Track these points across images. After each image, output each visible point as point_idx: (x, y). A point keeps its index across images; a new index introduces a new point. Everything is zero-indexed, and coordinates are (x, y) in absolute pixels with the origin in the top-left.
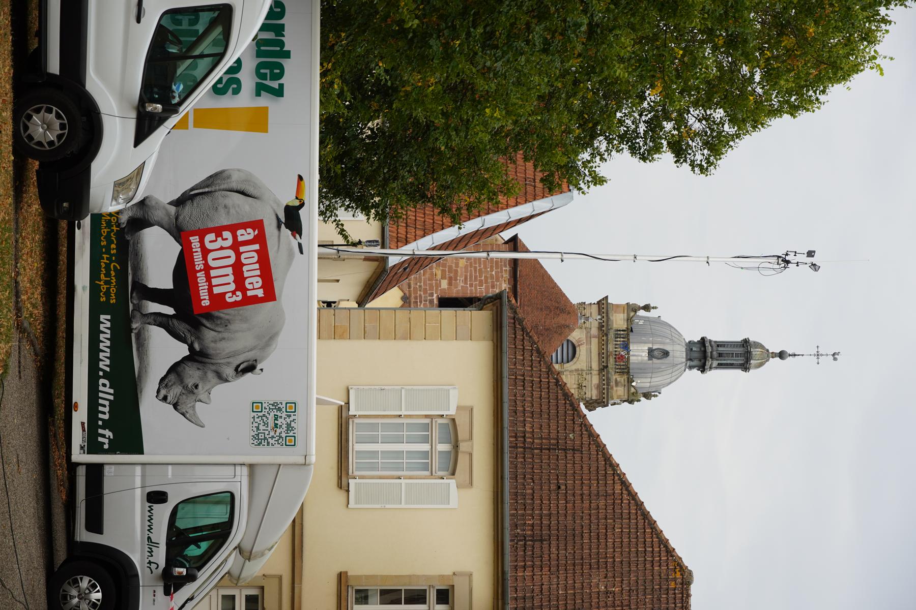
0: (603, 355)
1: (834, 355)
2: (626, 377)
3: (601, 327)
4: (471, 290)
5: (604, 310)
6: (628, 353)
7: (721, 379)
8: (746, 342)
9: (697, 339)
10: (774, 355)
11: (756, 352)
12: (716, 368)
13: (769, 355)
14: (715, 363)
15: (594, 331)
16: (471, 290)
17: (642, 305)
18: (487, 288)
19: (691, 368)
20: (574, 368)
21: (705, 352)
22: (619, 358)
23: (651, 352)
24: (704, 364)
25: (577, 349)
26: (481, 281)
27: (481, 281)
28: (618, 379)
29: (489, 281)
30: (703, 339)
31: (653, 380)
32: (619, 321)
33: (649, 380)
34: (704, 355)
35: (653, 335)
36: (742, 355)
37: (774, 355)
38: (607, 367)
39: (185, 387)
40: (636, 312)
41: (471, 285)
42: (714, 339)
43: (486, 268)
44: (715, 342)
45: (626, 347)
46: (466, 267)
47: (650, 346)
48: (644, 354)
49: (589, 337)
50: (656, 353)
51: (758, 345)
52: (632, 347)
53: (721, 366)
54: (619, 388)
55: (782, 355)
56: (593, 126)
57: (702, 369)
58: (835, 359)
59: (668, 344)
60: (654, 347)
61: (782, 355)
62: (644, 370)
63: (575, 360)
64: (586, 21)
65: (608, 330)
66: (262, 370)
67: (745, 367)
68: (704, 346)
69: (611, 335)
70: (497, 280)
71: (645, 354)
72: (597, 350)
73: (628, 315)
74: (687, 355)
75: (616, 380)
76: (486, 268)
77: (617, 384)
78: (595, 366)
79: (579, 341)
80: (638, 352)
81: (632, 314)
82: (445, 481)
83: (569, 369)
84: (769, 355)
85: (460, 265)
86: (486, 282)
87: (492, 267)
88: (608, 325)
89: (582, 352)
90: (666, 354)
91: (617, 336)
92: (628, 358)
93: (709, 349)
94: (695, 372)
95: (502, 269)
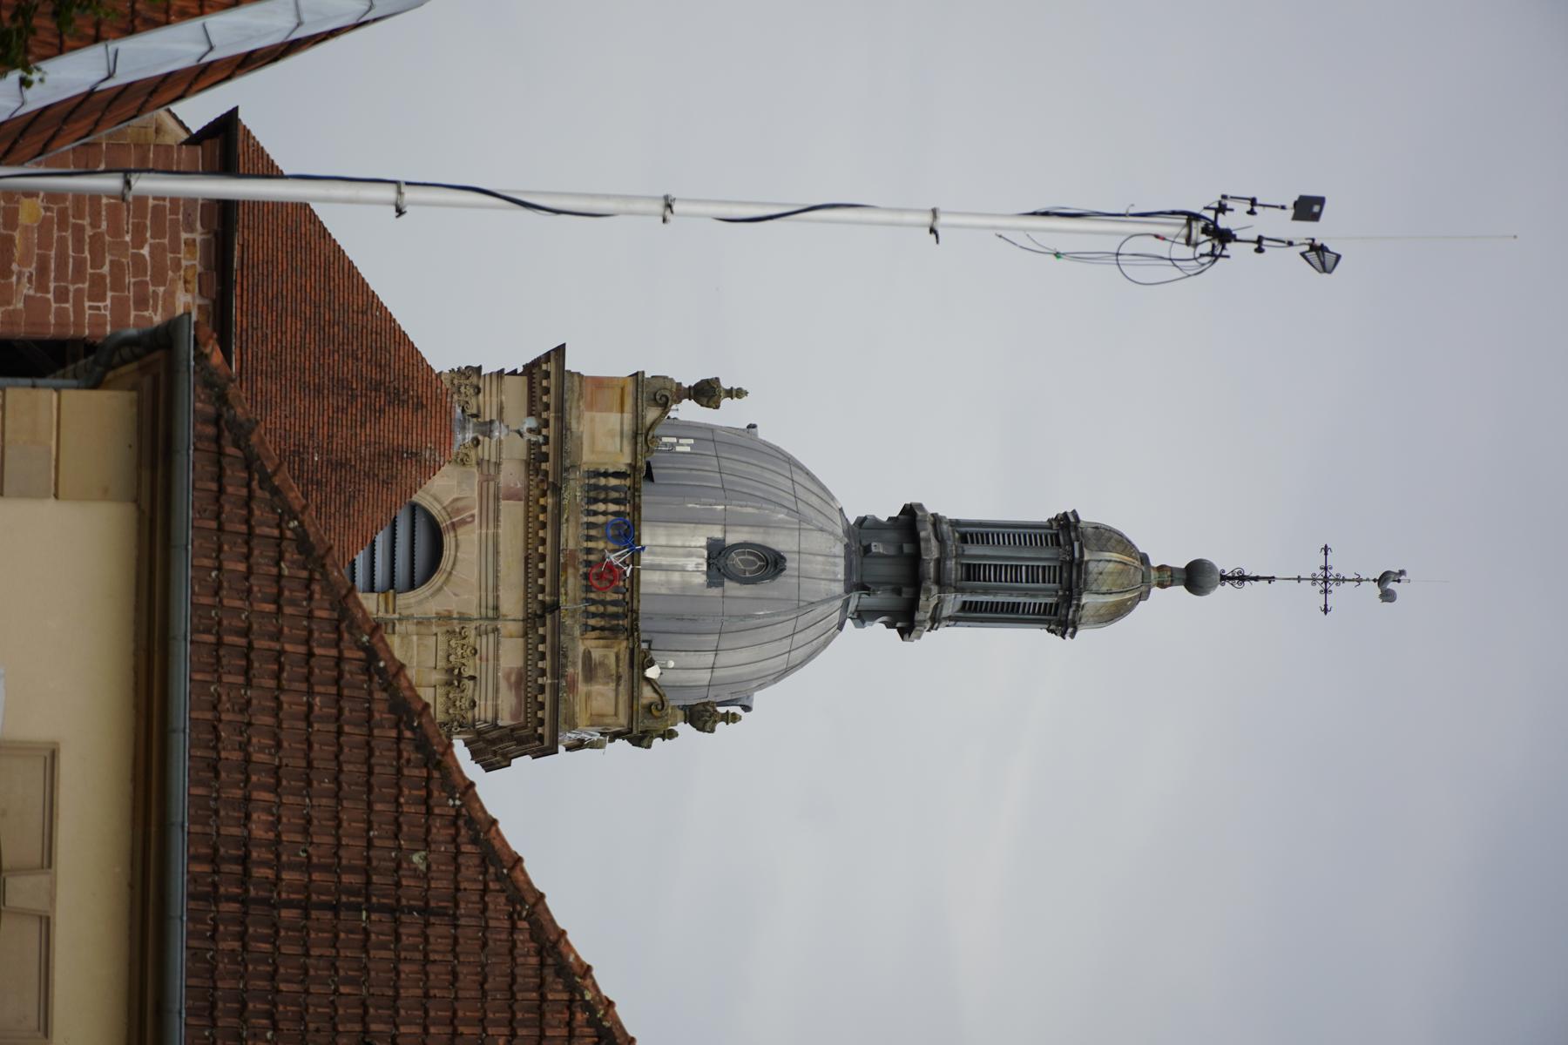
0: (541, 564)
1: (1383, 579)
2: (623, 646)
3: (535, 460)
4: (61, 313)
5: (550, 399)
6: (635, 558)
10: (1168, 577)
11: (1101, 563)
12: (954, 620)
13: (1147, 575)
14: (952, 602)
15: (512, 474)
16: (61, 313)
17: (689, 381)
18: (119, 306)
19: (862, 617)
20: (433, 607)
21: (915, 559)
22: (600, 575)
23: (717, 554)
25: (448, 540)
26: (97, 281)
27: (97, 281)
28: (596, 655)
29: (130, 279)
30: (910, 513)
31: (724, 658)
32: (602, 439)
33: (709, 658)
34: (912, 571)
35: (726, 492)
36: (1051, 574)
37: (1168, 577)
38: (555, 607)
40: (665, 407)
41: (61, 296)
42: (950, 512)
43: (116, 230)
44: (955, 524)
45: (627, 534)
46: (45, 226)
47: (717, 533)
48: (691, 563)
49: (492, 498)
50: (736, 560)
51: (1109, 538)
52: (649, 536)
53: (972, 613)
54: (596, 688)
55: (1195, 577)
57: (906, 622)
58: (1388, 596)
59: (779, 526)
61: (1195, 577)
62: (688, 622)
63: (438, 579)
65: (563, 470)
68: (914, 538)
69: (574, 490)
70: (159, 278)
71: (696, 565)
72: (520, 543)
73: (638, 416)
75: (587, 655)
76: (116, 230)
78: (512, 603)
79: (454, 509)
80: (673, 556)
81: (652, 414)
83: (417, 612)
84: (1147, 575)
85: (24, 218)
86: (118, 284)
87: (139, 231)
88: (561, 451)
90: (772, 563)
91: (594, 494)
93: (931, 551)
94: (879, 633)
95: (175, 239)
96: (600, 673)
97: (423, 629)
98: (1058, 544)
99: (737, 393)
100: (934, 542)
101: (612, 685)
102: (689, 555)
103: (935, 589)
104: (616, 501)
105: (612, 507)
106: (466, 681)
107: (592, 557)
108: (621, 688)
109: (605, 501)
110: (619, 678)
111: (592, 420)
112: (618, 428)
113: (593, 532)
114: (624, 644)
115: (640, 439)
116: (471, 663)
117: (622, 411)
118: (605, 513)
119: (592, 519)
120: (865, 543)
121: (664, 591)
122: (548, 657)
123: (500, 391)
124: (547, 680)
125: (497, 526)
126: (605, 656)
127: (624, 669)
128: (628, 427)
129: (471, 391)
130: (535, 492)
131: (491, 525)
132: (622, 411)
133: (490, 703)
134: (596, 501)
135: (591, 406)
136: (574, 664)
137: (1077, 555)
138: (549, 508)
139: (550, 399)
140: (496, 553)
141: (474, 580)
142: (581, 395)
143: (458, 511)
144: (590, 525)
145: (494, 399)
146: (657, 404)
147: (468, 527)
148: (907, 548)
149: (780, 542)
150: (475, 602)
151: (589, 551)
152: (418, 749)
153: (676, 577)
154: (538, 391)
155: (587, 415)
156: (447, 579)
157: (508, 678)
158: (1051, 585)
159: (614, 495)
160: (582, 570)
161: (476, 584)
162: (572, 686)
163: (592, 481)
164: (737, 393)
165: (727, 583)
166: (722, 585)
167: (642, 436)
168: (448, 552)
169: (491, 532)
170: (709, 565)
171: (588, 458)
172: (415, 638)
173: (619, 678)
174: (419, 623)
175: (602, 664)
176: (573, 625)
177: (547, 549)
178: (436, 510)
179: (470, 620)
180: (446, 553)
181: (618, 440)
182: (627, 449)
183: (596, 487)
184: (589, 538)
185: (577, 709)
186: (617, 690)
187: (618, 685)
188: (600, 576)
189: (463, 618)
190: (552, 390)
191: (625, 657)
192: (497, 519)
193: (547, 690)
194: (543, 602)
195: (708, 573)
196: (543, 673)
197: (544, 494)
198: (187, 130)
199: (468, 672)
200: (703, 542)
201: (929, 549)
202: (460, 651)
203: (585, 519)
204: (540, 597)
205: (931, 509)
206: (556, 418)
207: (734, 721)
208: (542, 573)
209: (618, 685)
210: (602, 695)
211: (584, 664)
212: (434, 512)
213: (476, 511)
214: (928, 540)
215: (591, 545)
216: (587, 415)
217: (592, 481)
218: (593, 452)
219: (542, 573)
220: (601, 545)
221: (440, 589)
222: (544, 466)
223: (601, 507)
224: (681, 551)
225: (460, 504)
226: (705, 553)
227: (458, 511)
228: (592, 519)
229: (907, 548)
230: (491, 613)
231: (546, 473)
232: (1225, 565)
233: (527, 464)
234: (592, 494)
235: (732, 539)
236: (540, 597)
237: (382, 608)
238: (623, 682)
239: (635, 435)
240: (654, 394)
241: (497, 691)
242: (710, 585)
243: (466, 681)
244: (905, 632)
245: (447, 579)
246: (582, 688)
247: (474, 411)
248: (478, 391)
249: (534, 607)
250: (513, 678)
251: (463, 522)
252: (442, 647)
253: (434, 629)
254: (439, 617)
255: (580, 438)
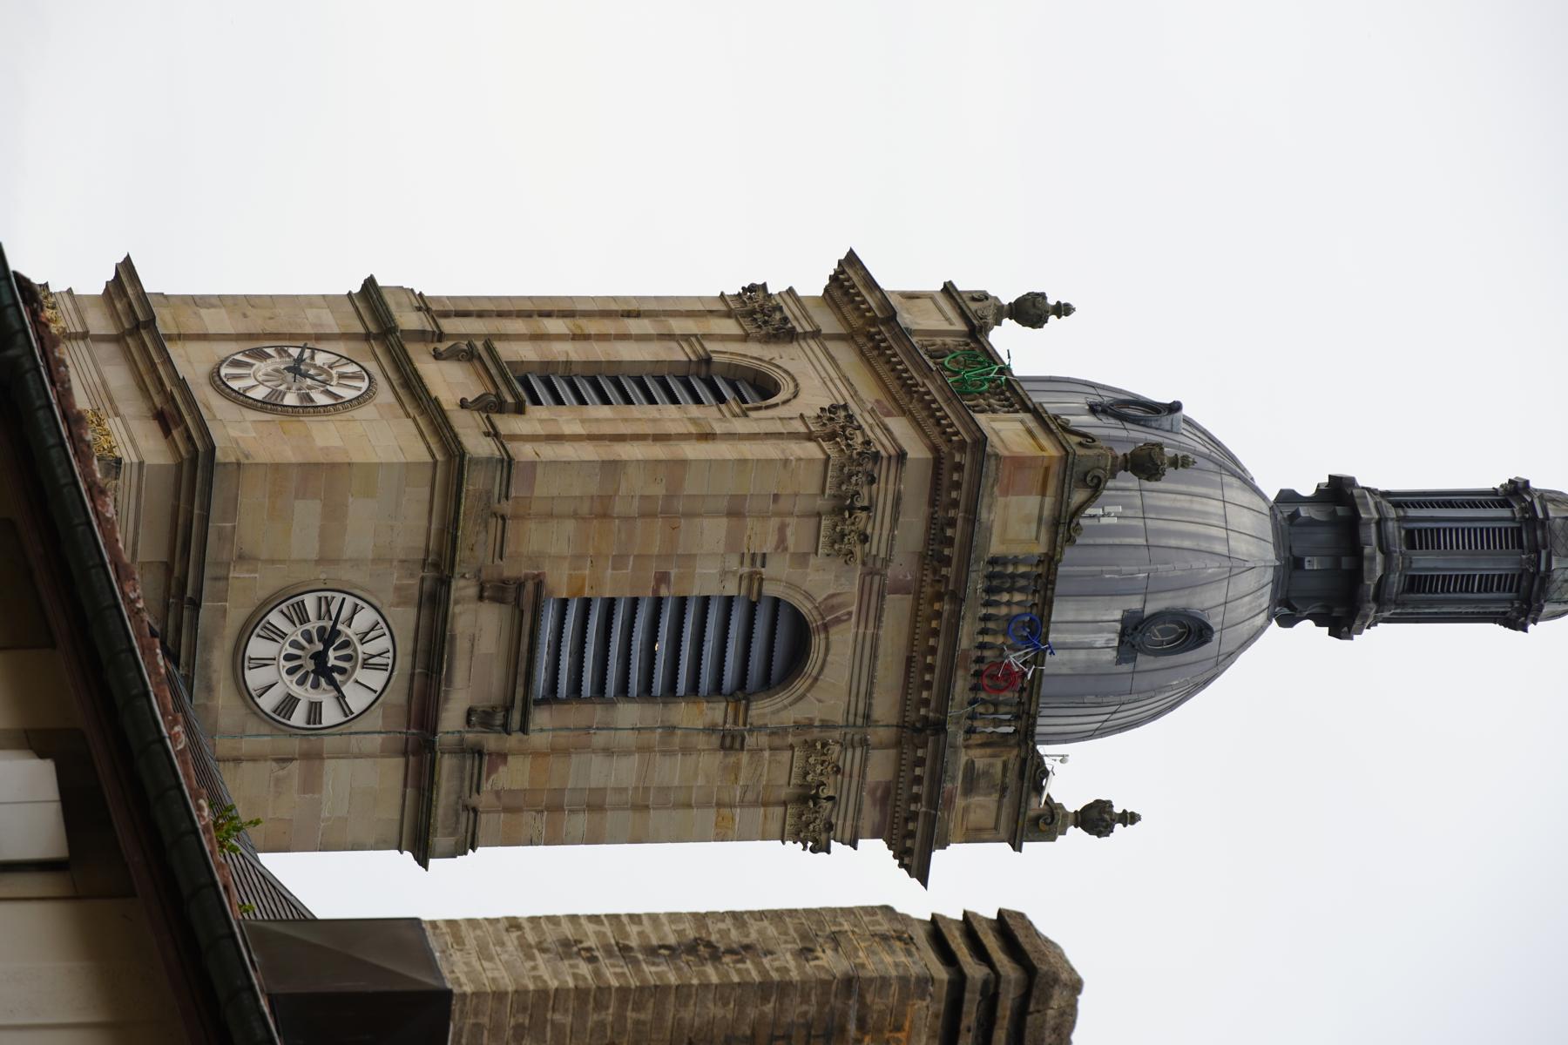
0: (925, 664)
6: (1038, 660)
15: (902, 567)
17: (1007, 298)
18: (821, 1005)
19: (1287, 612)
20: (790, 716)
21: (1355, 575)
22: (991, 677)
25: (817, 642)
28: (980, 764)
38: (939, 727)
45: (1035, 632)
47: (1135, 603)
48: (1100, 640)
54: (976, 799)
56: (1329, 484)
60: (1151, 609)
63: (800, 685)
65: (965, 563)
68: (1356, 550)
69: (976, 582)
71: (1107, 638)
72: (903, 640)
73: (1061, 500)
74: (1276, 582)
75: (970, 765)
77: (972, 781)
78: (885, 707)
79: (829, 606)
80: (1083, 630)
83: (773, 722)
89: (836, 655)
92: (1038, 675)
96: (983, 783)
97: (777, 741)
98: (1521, 546)
100: (1379, 557)
101: (995, 796)
102: (1101, 631)
103: (1373, 606)
104: (1022, 590)
105: (1018, 597)
106: (824, 803)
107: (987, 653)
108: (1005, 800)
109: (1010, 591)
110: (1004, 790)
111: (1006, 506)
112: (1036, 512)
113: (991, 625)
114: (1015, 752)
115: (1061, 529)
116: (831, 781)
117: (1043, 494)
118: (1009, 603)
119: (991, 611)
120: (1296, 552)
121: (1065, 671)
122: (926, 782)
123: (898, 479)
124: (921, 808)
125: (877, 626)
126: (991, 765)
127: (1012, 778)
128: (1046, 513)
129: (862, 478)
130: (928, 590)
131: (871, 625)
132: (1043, 494)
133: (849, 823)
134: (999, 590)
135: (1005, 493)
136: (954, 778)
137: (1543, 568)
138: (945, 615)
139: (918, 827)
140: (874, 656)
141: (843, 683)
142: (996, 480)
143: (833, 609)
144: (986, 618)
145: (891, 487)
146: (1086, 486)
147: (842, 626)
148: (1346, 563)
149: (1203, 601)
150: (842, 706)
151: (982, 646)
152: (765, 999)
153: (1081, 655)
154: (945, 482)
155: (1001, 500)
156: (812, 686)
157: (873, 792)
158: (1507, 595)
159: (1022, 583)
160: (974, 667)
161: (845, 688)
162: (950, 802)
163: (997, 569)
165: (1140, 658)
166: (1134, 659)
167: (1064, 525)
168: (816, 655)
169: (870, 632)
170: (1121, 642)
171: (996, 548)
172: (767, 754)
173: (1004, 790)
174: (773, 734)
175: (986, 773)
176: (956, 733)
177: (938, 660)
178: (805, 608)
179: (834, 727)
180: (813, 656)
181: (1034, 526)
182: (1044, 537)
183: (1000, 575)
184: (984, 632)
185: (952, 826)
186: (1000, 802)
187: (1002, 796)
188: (993, 677)
189: (826, 726)
190: (964, 486)
191: (1014, 766)
192: (878, 618)
193: (921, 818)
194: (926, 718)
195: (1118, 649)
196: (916, 798)
197: (939, 597)
199: (828, 792)
200: (1118, 615)
201: (1372, 570)
202: (819, 768)
203: (984, 611)
204: (923, 711)
206: (966, 520)
207: (1133, 823)
208: (928, 686)
209: (1002, 796)
210: (982, 807)
211: (965, 776)
212: (804, 611)
213: (854, 608)
214: (1373, 558)
215: (988, 639)
216: (1001, 500)
217: (997, 569)
218: (1003, 542)
219: (928, 686)
220: (1000, 640)
221: (802, 697)
222: (944, 571)
223: (1005, 597)
224: (1090, 626)
225: (835, 601)
226: (1119, 626)
227: (833, 609)
228: (991, 611)
229: (1346, 563)
230: (859, 721)
231: (946, 578)
233: (922, 557)
234: (995, 583)
236: (923, 711)
237: (730, 719)
238: (1008, 794)
239: (1056, 523)
241: (858, 811)
242: (1119, 662)
243: (824, 803)
245: (812, 686)
246: (960, 802)
247: (866, 503)
248: (872, 480)
249: (911, 716)
250: (879, 793)
251: (838, 621)
252: (798, 763)
253: (790, 739)
254: (798, 726)
255: (990, 529)
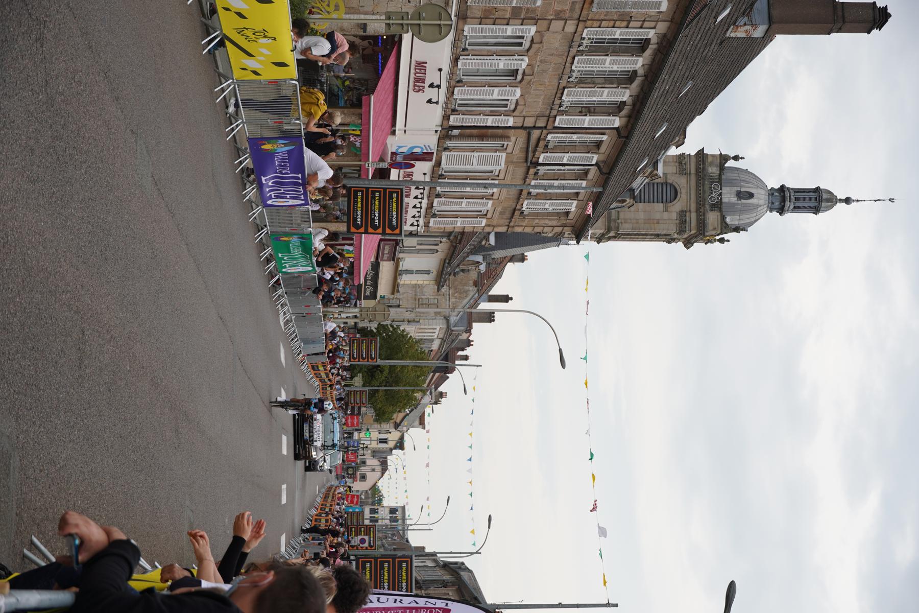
7: (806, 219)
8: (817, 190)
9: (777, 187)
10: (841, 200)
14: (792, 207)
17: (732, 155)
24: (784, 206)
30: (783, 187)
32: (713, 170)
34: (785, 200)
36: (815, 200)
37: (841, 200)
39: (512, 162)
42: (791, 187)
55: (848, 201)
57: (781, 211)
61: (848, 201)
62: (733, 208)
64: (594, 9)
66: (474, 544)
67: (816, 210)
68: (784, 192)
82: (498, 154)
90: (751, 195)
93: (787, 195)
94: (775, 214)
99: (742, 158)
149: (752, 191)
164: (742, 158)
198: (428, 272)
205: (787, 186)
232: (854, 198)
235: (743, 190)
240: (724, 158)
244: (781, 214)
